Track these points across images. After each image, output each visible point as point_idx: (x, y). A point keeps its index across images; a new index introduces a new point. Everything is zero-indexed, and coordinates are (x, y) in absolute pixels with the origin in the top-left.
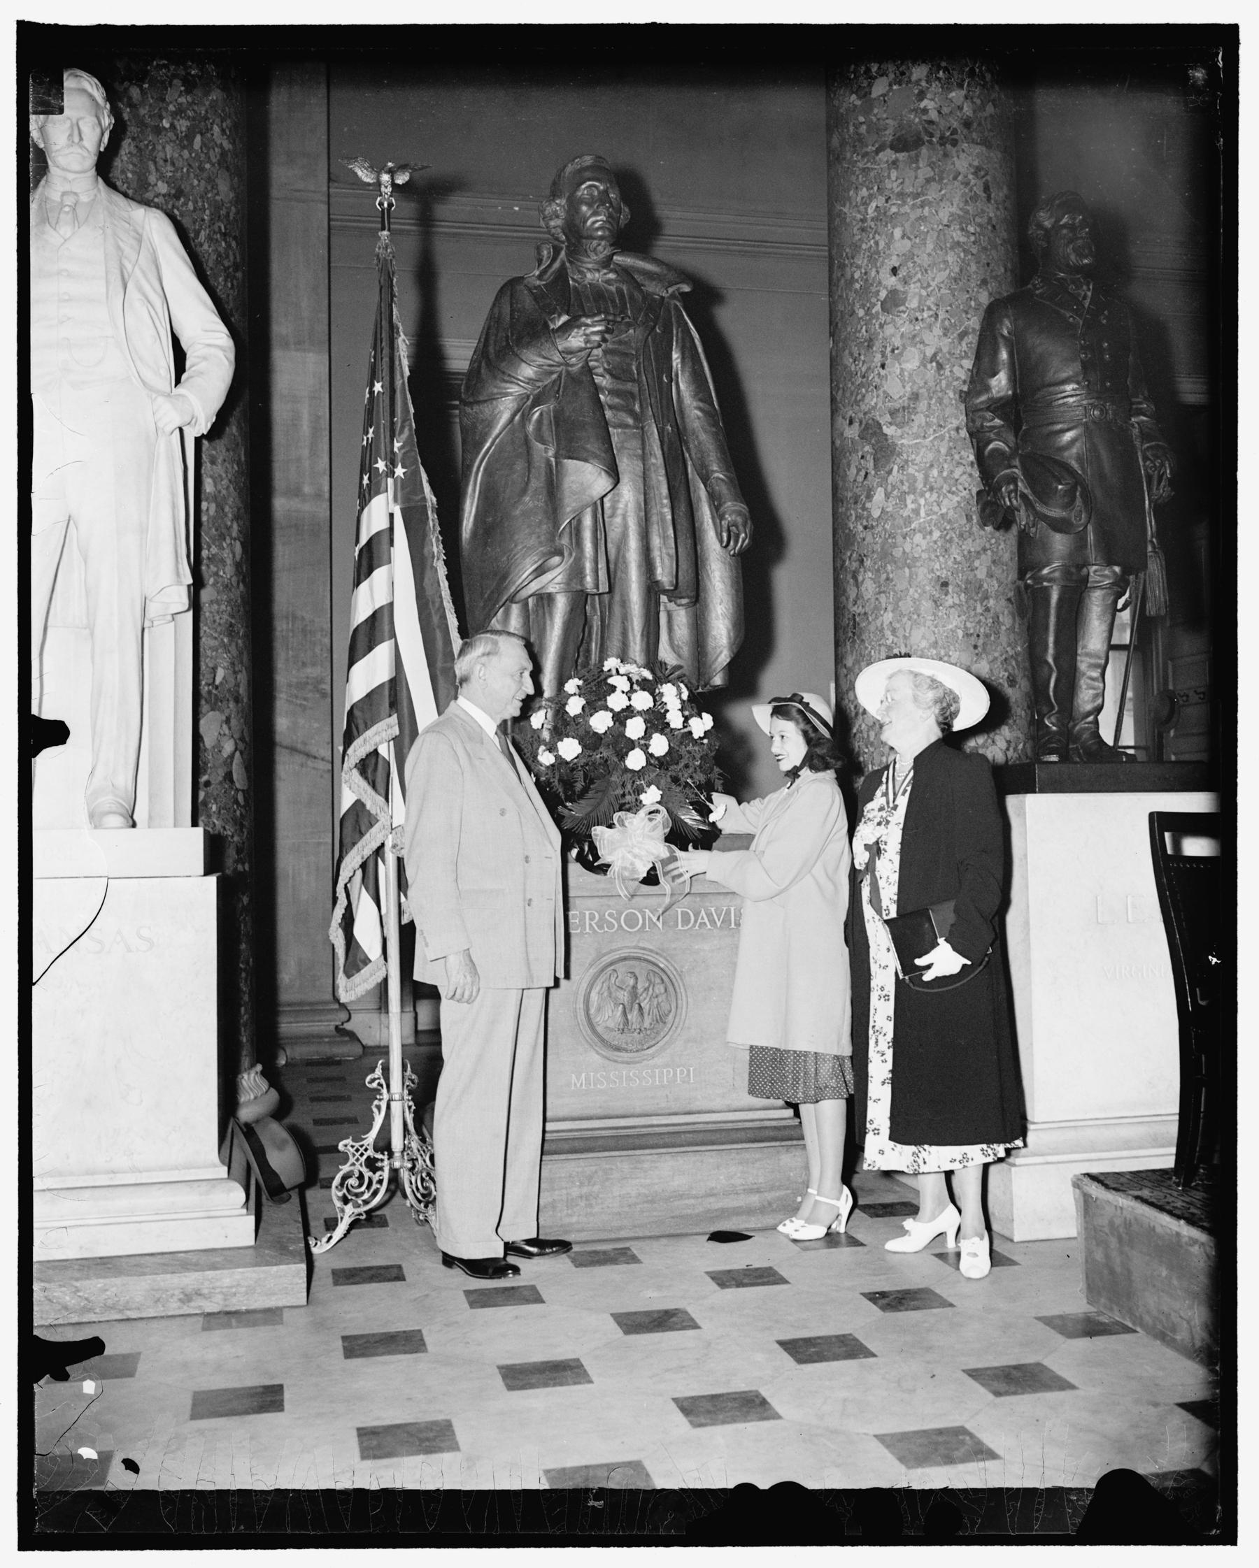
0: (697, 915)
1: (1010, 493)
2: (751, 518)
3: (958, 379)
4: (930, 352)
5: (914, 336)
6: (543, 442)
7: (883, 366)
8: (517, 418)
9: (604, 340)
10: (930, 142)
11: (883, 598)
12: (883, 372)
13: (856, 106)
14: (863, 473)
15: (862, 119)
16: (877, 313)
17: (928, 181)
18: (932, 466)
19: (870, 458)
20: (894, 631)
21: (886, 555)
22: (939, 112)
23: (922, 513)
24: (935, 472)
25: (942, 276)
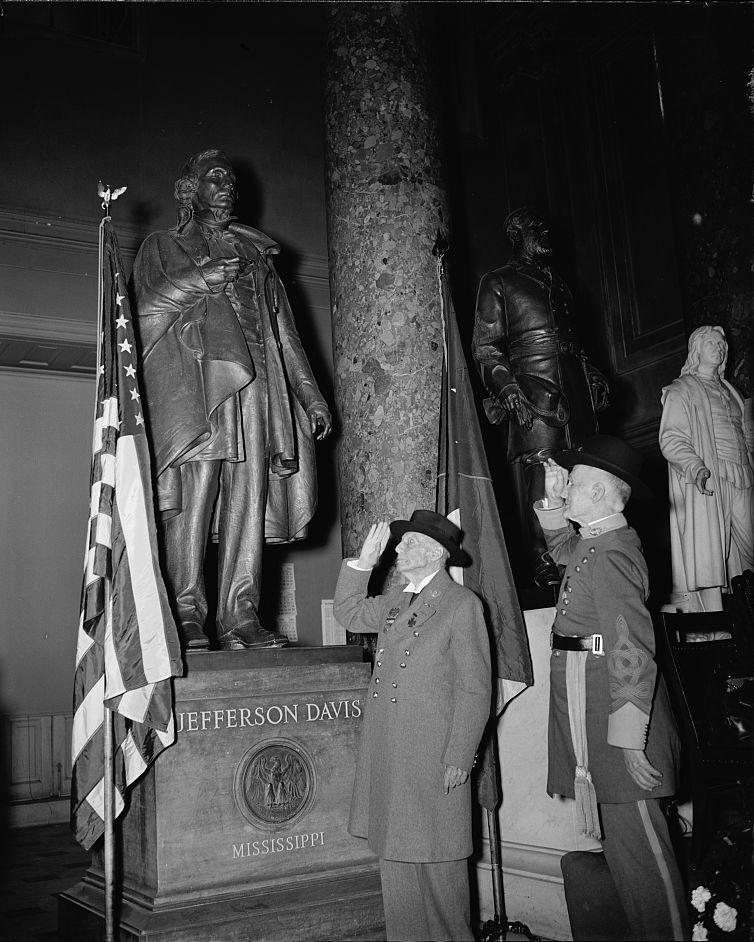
0: (321, 709)
1: (514, 400)
3: (430, 334)
4: (411, 316)
5: (400, 305)
6: (192, 347)
7: (379, 324)
8: (170, 329)
9: (237, 277)
10: (406, 180)
11: (385, 482)
12: (379, 328)
13: (352, 154)
14: (366, 396)
15: (357, 162)
16: (374, 289)
17: (405, 204)
18: (416, 391)
19: (372, 386)
20: (394, 505)
21: (386, 452)
22: (410, 162)
23: (411, 424)
24: (418, 396)
25: (416, 267)
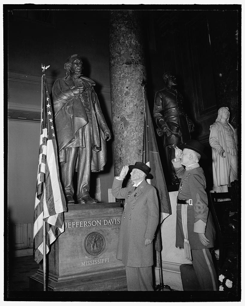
0: (108, 221)
1: (166, 129)
2: (225, 107)
3: (141, 109)
4: (135, 104)
5: (132, 101)
6: (69, 113)
7: (125, 106)
8: (63, 108)
9: (83, 92)
10: (133, 63)
11: (127, 154)
12: (125, 107)
13: (117, 56)
14: (122, 128)
15: (119, 58)
16: (124, 96)
17: (133, 71)
18: (136, 127)
19: (123, 125)
20: (130, 160)
21: (127, 145)
22: (135, 58)
23: (135, 136)
24: (137, 128)
25: (136, 89)
